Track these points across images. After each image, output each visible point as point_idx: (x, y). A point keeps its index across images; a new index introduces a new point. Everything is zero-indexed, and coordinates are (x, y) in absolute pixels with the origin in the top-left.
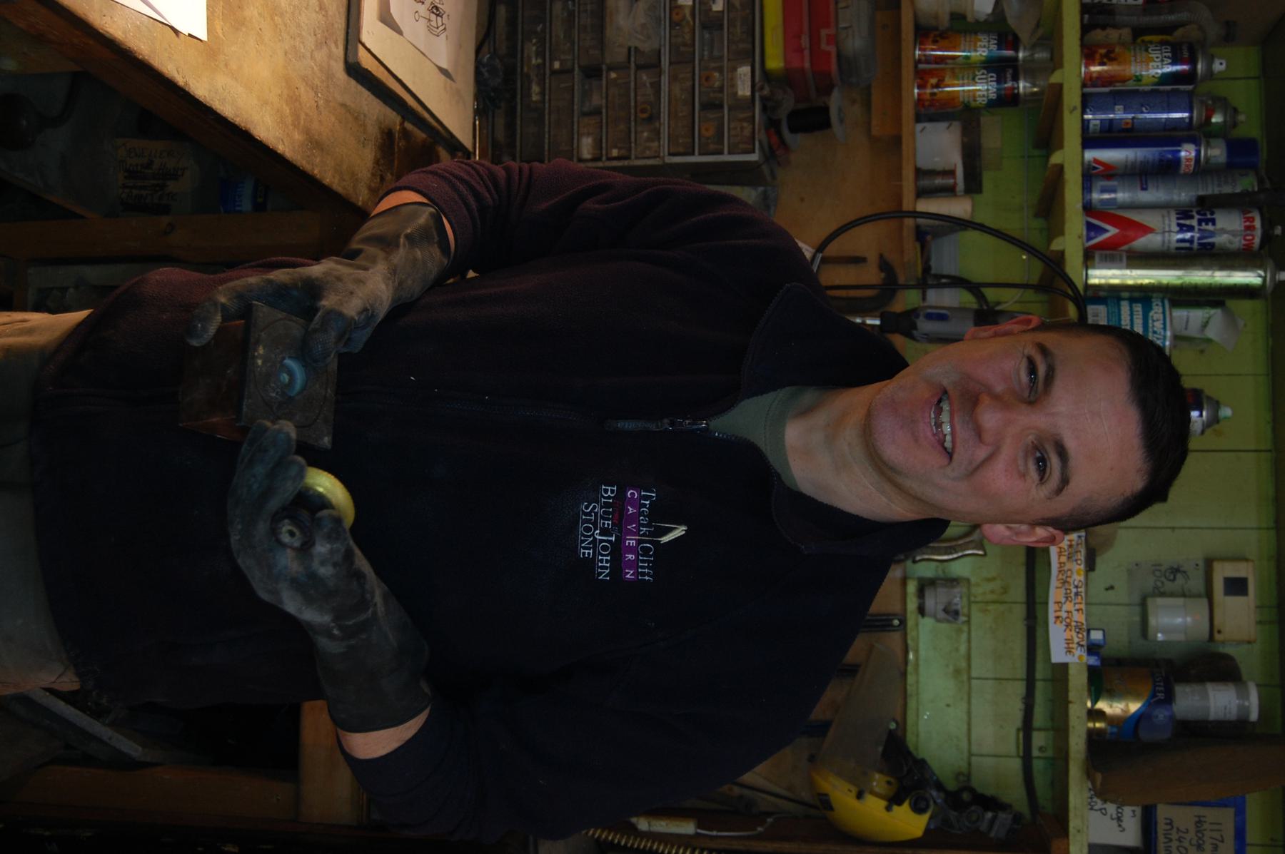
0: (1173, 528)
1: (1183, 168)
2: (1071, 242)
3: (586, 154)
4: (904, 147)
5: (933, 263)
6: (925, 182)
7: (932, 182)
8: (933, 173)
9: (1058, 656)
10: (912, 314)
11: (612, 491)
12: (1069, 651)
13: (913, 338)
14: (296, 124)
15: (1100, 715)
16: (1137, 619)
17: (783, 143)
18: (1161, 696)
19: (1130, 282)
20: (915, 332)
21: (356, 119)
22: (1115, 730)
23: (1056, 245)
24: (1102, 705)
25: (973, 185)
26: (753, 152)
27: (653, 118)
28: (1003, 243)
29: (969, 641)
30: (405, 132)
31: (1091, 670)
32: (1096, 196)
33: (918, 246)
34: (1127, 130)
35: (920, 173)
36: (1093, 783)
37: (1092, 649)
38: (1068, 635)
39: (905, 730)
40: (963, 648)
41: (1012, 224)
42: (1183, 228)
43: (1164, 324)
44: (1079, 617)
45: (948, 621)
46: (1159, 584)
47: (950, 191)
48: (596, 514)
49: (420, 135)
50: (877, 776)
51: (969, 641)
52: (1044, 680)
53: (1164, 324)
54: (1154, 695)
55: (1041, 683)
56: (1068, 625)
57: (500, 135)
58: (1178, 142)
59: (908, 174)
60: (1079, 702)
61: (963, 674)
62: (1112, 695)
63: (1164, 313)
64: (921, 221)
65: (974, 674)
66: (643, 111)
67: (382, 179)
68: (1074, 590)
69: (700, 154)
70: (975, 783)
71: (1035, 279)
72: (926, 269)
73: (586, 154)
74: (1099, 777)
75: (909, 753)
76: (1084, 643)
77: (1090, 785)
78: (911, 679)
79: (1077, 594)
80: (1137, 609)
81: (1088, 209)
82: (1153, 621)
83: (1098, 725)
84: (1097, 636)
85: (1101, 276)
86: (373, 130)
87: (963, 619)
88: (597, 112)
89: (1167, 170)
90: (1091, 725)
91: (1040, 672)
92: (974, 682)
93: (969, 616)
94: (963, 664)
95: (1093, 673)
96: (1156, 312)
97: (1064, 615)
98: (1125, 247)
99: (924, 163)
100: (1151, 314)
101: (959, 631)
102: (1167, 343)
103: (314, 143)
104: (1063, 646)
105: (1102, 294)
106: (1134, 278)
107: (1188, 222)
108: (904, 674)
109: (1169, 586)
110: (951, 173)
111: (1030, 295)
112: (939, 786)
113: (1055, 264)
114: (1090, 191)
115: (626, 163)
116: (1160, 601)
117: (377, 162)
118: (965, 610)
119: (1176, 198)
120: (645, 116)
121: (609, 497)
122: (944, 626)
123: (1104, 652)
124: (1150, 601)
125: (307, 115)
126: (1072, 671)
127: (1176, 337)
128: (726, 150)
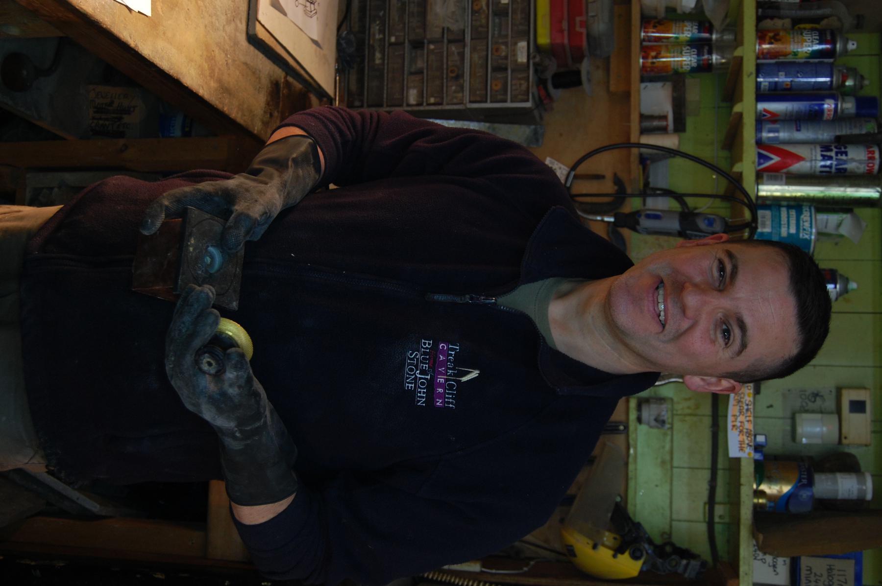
1: (826, 117)
2: (747, 166)
3: (412, 100)
4: (632, 99)
6: (647, 124)
7: (651, 124)
8: (652, 117)
9: (734, 452)
10: (636, 214)
12: (741, 449)
15: (762, 494)
16: (789, 428)
17: (549, 96)
18: (805, 481)
19: (788, 195)
20: (638, 227)
21: (254, 73)
22: (772, 504)
23: (737, 168)
24: (764, 487)
25: (680, 126)
26: (527, 101)
27: (459, 77)
29: (672, 441)
31: (756, 462)
33: (641, 167)
35: (643, 117)
36: (757, 542)
37: (758, 448)
38: (740, 438)
40: (668, 447)
42: (825, 158)
44: (749, 426)
45: (658, 428)
46: (804, 404)
47: (663, 130)
48: (417, 359)
49: (298, 86)
50: (607, 534)
51: (672, 441)
52: (723, 469)
54: (800, 480)
55: (721, 471)
56: (741, 431)
57: (354, 87)
58: (823, 98)
61: (667, 464)
62: (771, 480)
63: (811, 216)
64: (643, 150)
65: (675, 464)
66: (452, 72)
67: (271, 115)
68: (746, 407)
69: (491, 102)
70: (675, 540)
72: (646, 184)
73: (412, 100)
74: (761, 537)
75: (629, 518)
76: (752, 444)
77: (754, 542)
78: (631, 467)
79: (747, 410)
80: (789, 421)
81: (759, 143)
82: (799, 430)
83: (761, 501)
84: (761, 439)
85: (768, 190)
86: (265, 82)
87: (668, 426)
88: (420, 72)
89: (814, 117)
90: (756, 501)
91: (720, 464)
92: (675, 470)
93: (672, 424)
94: (668, 458)
96: (805, 216)
98: (785, 170)
99: (645, 111)
100: (802, 217)
101: (665, 434)
102: (813, 237)
103: (224, 89)
104: (738, 446)
105: (768, 202)
107: (828, 154)
108: (627, 464)
109: (811, 406)
110: (664, 118)
111: (718, 202)
112: (650, 542)
113: (736, 181)
115: (440, 107)
117: (268, 104)
118: (670, 420)
119: (820, 137)
120: (453, 75)
124: (798, 416)
125: (220, 69)
127: (820, 234)
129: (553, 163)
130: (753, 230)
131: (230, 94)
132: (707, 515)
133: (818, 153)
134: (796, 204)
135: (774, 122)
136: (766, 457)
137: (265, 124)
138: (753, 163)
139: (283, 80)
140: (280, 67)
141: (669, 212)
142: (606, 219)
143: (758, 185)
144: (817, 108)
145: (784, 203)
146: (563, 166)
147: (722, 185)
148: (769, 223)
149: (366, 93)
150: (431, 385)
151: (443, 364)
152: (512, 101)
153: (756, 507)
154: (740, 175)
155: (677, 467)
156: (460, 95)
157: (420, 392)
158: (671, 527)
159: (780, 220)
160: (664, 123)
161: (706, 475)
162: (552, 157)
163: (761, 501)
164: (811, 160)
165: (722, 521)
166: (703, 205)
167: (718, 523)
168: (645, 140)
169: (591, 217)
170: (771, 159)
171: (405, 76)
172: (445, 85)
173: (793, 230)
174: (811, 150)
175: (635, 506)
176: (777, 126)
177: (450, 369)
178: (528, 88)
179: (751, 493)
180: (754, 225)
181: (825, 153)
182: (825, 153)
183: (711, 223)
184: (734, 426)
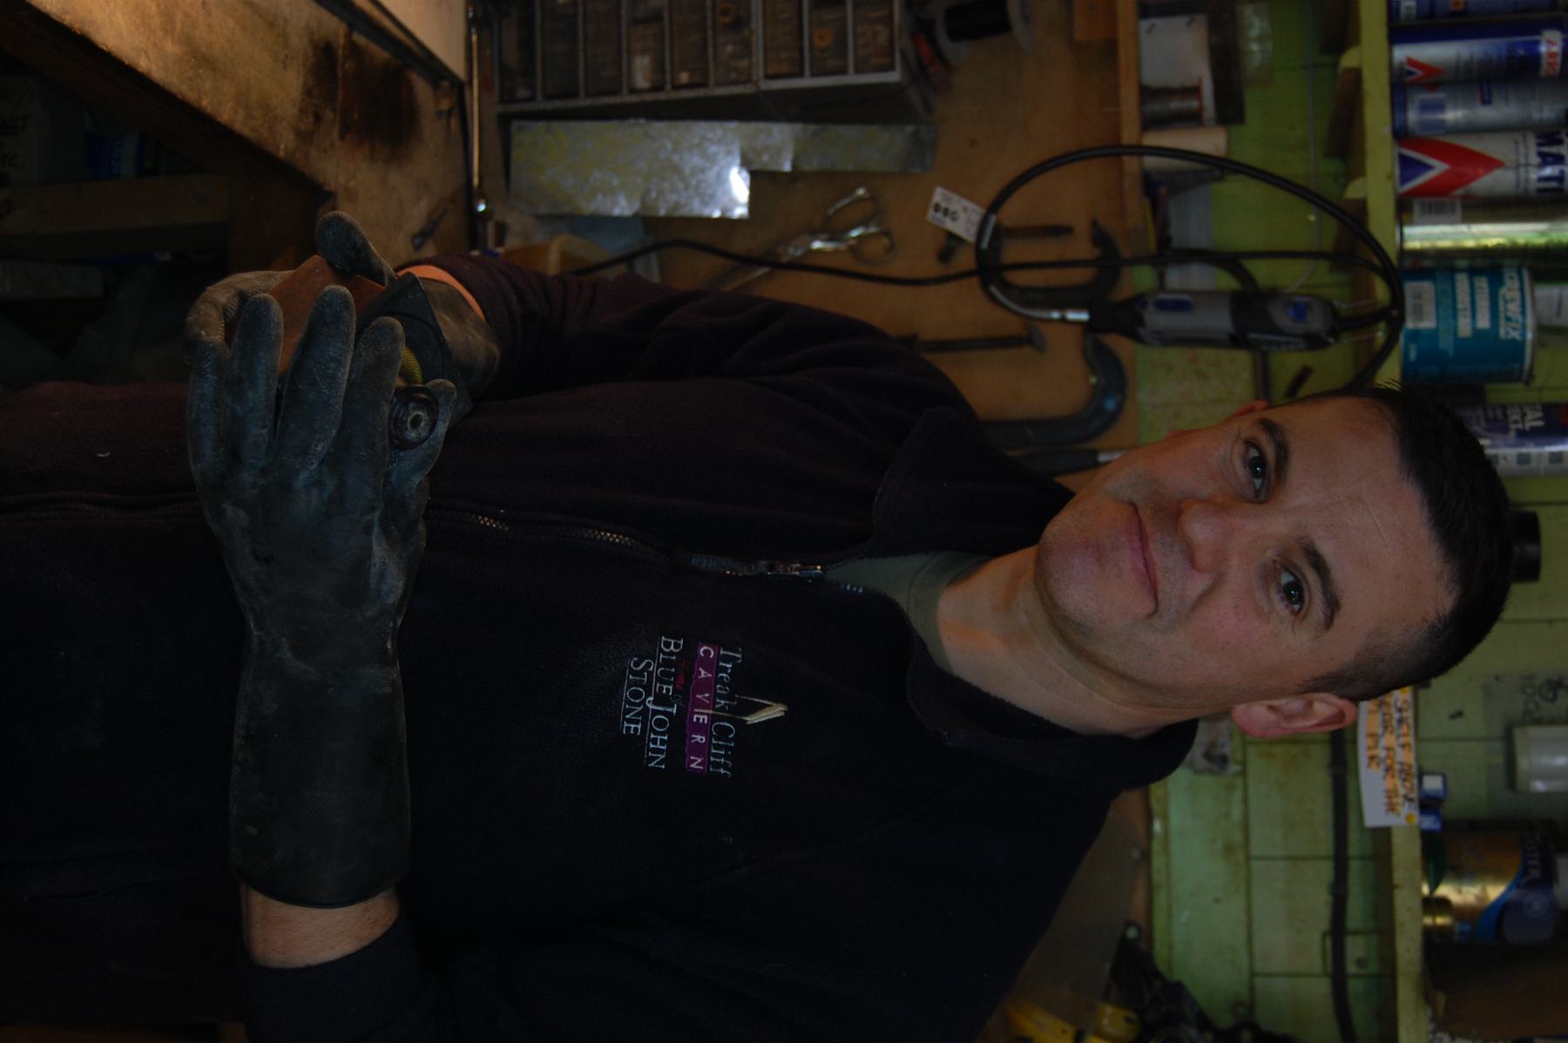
0: (1550, 622)
1: (1545, 69)
2: (1376, 186)
3: (641, 82)
4: (1122, 54)
5: (1174, 231)
6: (1156, 107)
7: (1165, 106)
8: (1167, 92)
9: (1374, 813)
10: (1138, 301)
11: (677, 646)
12: (1391, 808)
13: (1137, 338)
14: (168, 27)
15: (1443, 905)
16: (1499, 760)
17: (940, 56)
18: (1535, 873)
19: (1470, 243)
20: (1142, 331)
21: (271, 24)
22: (1467, 928)
23: (1354, 191)
24: (1445, 890)
25: (1230, 111)
26: (891, 68)
27: (739, 23)
28: (1281, 195)
29: (1245, 800)
30: (353, 49)
31: (1426, 836)
32: (1413, 116)
33: (1147, 203)
34: (1455, 14)
35: (1147, 93)
36: (1434, 1009)
37: (1428, 804)
38: (1389, 783)
39: (1150, 940)
40: (1237, 814)
41: (1294, 167)
42: (1546, 159)
43: (1523, 306)
44: (1406, 757)
45: (1211, 772)
46: (1532, 706)
47: (1192, 119)
48: (650, 674)
49: (380, 54)
50: (1109, 1010)
51: (1245, 800)
52: (1362, 858)
53: (1523, 306)
54: (1524, 873)
55: (1355, 857)
56: (1388, 769)
57: (512, 57)
58: (1536, 28)
59: (1129, 95)
60: (1411, 888)
61: (1238, 852)
62: (1461, 874)
63: (1522, 289)
64: (1150, 162)
65: (1255, 851)
66: (725, 12)
67: (318, 118)
68: (1396, 715)
69: (813, 75)
70: (1264, 1020)
71: (1328, 243)
72: (1164, 240)
73: (641, 82)
74: (1441, 998)
75: (1157, 974)
76: (1414, 795)
77: (1429, 1013)
78: (1158, 861)
79: (1401, 721)
80: (1499, 746)
81: (1401, 135)
82: (1523, 763)
83: (1440, 920)
84: (1433, 784)
85: (1424, 235)
86: (299, 43)
87: (1234, 768)
88: (656, 17)
89: (1518, 72)
90: (1428, 921)
91: (1355, 846)
92: (1255, 864)
93: (1244, 764)
94: (1237, 837)
95: (1431, 844)
96: (1510, 289)
97: (1382, 753)
98: (1460, 192)
99: (1154, 76)
100: (1503, 291)
101: (1230, 788)
102: (1529, 336)
103: (201, 59)
104: (1382, 801)
105: (1426, 263)
106: (1475, 237)
107: (1554, 150)
108: (1147, 855)
109: (1547, 709)
110: (1195, 91)
111: (1323, 266)
112: (1204, 1023)
113: (1353, 218)
114: (1404, 109)
115: (701, 93)
116: (1535, 732)
117: (308, 92)
118: (1238, 756)
119: (1536, 116)
120: (727, 20)
121: (672, 653)
122: (1207, 780)
123: (1449, 809)
124: (1518, 733)
125: (186, 14)
126: (1398, 839)
127: (1543, 329)
128: (851, 68)
129: (948, 200)
130: (1396, 324)
131: (214, 70)
132: (1329, 961)
133: (1530, 149)
134: (1489, 263)
135: (1433, 86)
136: (1447, 825)
137: (305, 137)
138: (1390, 177)
139: (342, 41)
140: (334, 13)
141: (1209, 296)
142: (1072, 316)
143: (1402, 225)
144: (1521, 52)
145: (1462, 263)
146: (970, 205)
147: (1327, 233)
148: (1429, 308)
149: (539, 69)
150: (679, 728)
151: (704, 686)
152: (858, 71)
153: (1429, 934)
154: (1362, 205)
155: (1261, 858)
156: (743, 63)
157: (663, 742)
158: (1252, 989)
159: (1454, 301)
160: (1194, 104)
161: (1324, 872)
162: (946, 186)
163: (1440, 920)
164: (1517, 167)
165: (1362, 971)
166: (1289, 276)
167: (1356, 976)
168: (1151, 139)
169: (1037, 313)
170: (1429, 167)
171: (624, 29)
172: (710, 42)
173: (1484, 322)
174: (1516, 143)
175: (1170, 947)
176: (1439, 95)
177: (722, 697)
178: (891, 41)
179: (1417, 905)
180: (1395, 313)
181: (1546, 149)
182: (1546, 149)
183: (1300, 312)
184: (1372, 758)
